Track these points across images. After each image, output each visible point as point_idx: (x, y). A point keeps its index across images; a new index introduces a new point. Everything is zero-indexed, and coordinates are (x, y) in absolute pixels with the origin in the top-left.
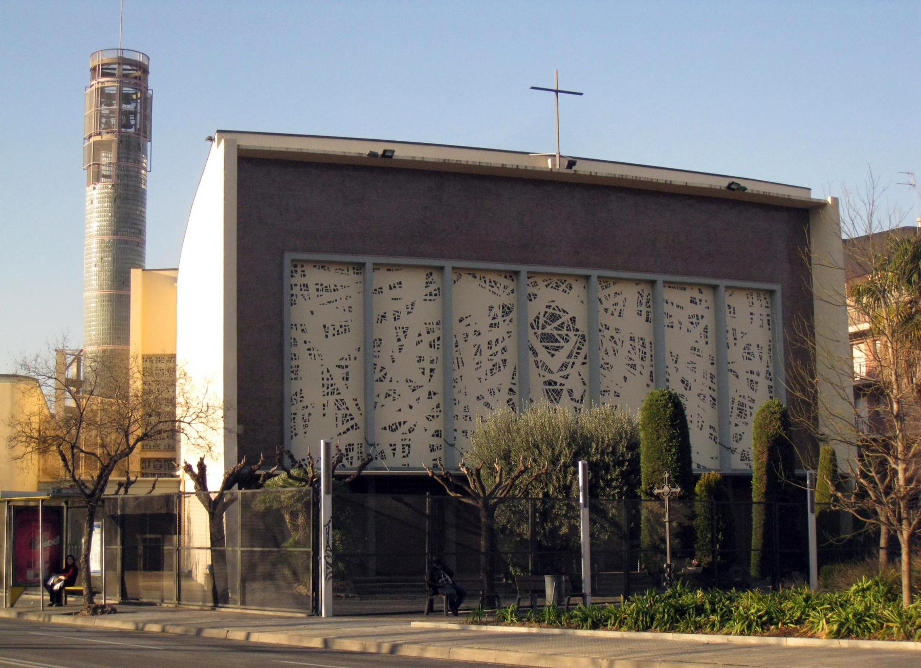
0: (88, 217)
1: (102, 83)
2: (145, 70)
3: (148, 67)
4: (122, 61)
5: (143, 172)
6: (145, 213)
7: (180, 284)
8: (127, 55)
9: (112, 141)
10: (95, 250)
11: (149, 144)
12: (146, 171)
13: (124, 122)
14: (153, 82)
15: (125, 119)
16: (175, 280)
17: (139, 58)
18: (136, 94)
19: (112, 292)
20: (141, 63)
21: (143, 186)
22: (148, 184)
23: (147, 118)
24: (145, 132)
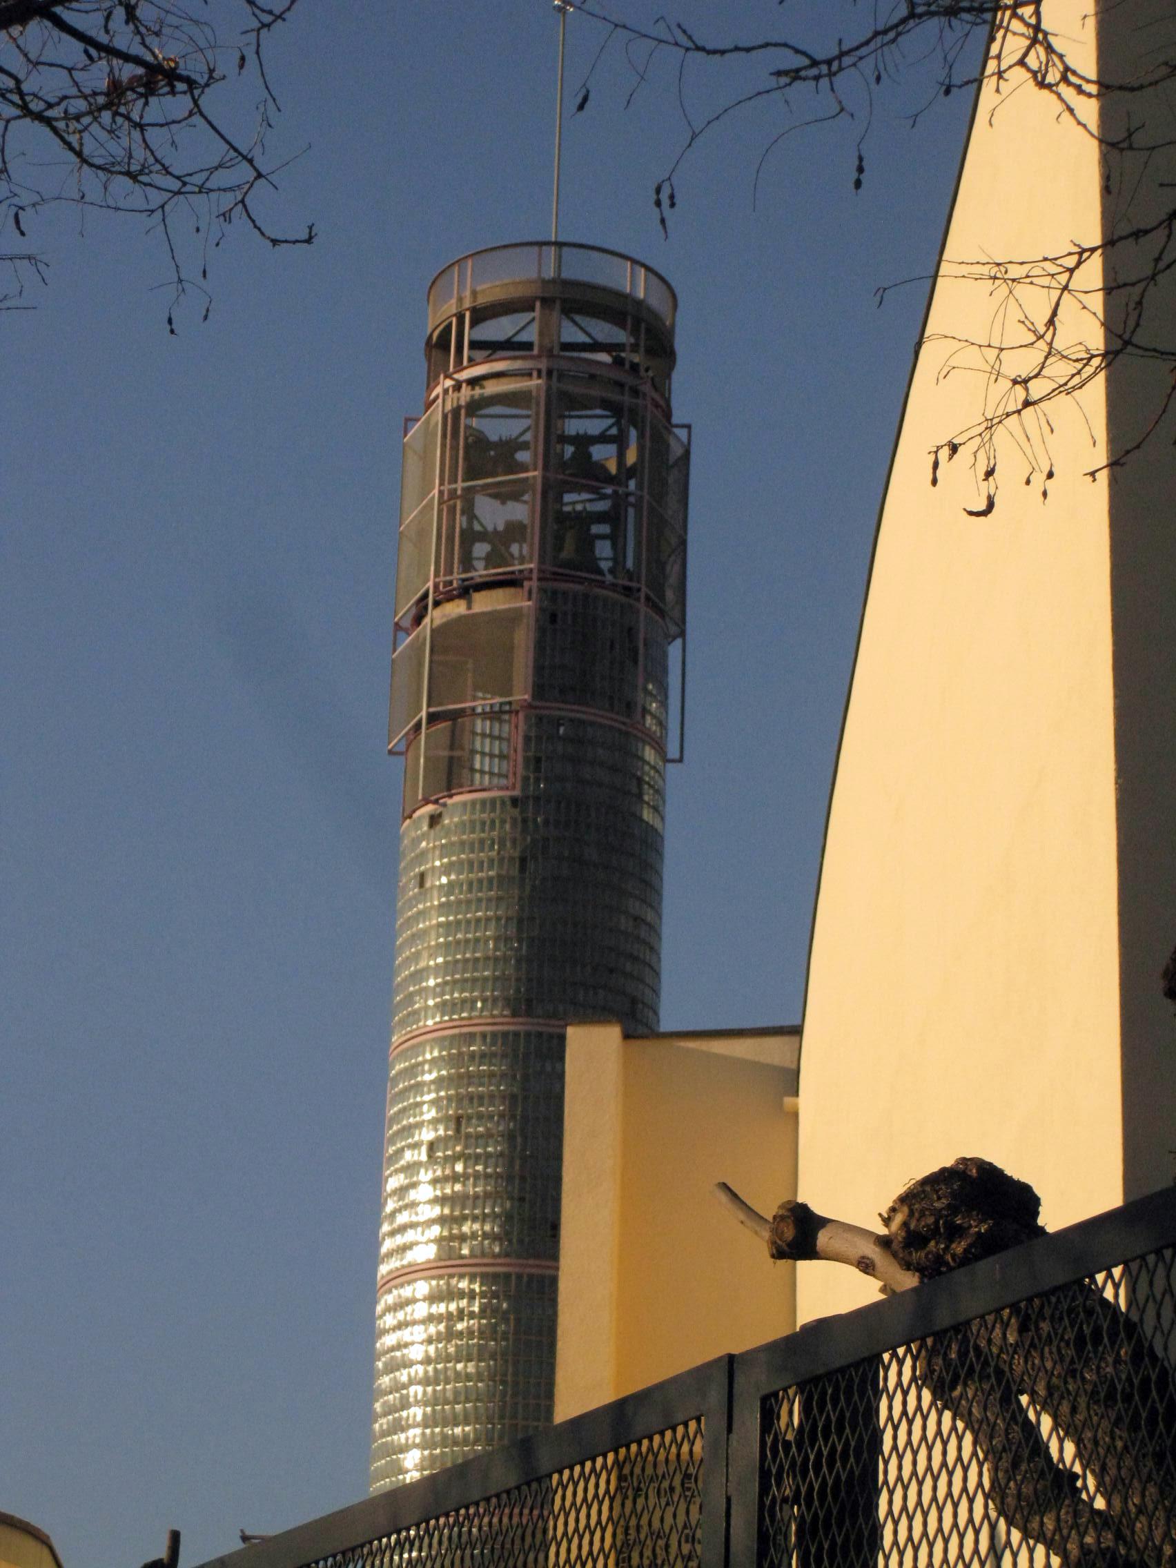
0: (381, 1424)
1: (474, 382)
2: (657, 341)
3: (671, 332)
4: (572, 299)
5: (649, 754)
6: (654, 930)
7: (808, 1102)
8: (581, 269)
9: (509, 619)
10: (430, 1113)
11: (674, 650)
12: (660, 748)
13: (568, 552)
14: (695, 394)
15: (566, 540)
16: (790, 1080)
17: (640, 287)
18: (621, 442)
19: (519, 1025)
20: (639, 303)
21: (647, 815)
22: (671, 810)
23: (666, 544)
24: (657, 585)
